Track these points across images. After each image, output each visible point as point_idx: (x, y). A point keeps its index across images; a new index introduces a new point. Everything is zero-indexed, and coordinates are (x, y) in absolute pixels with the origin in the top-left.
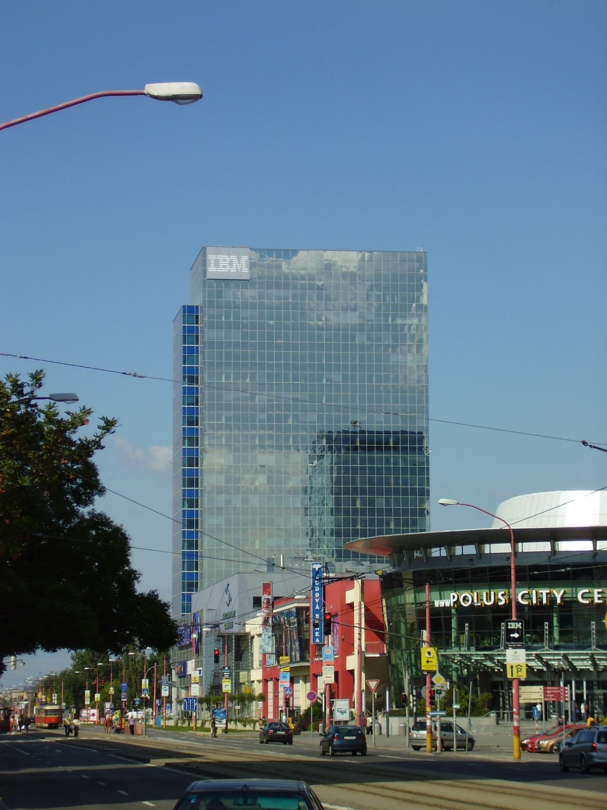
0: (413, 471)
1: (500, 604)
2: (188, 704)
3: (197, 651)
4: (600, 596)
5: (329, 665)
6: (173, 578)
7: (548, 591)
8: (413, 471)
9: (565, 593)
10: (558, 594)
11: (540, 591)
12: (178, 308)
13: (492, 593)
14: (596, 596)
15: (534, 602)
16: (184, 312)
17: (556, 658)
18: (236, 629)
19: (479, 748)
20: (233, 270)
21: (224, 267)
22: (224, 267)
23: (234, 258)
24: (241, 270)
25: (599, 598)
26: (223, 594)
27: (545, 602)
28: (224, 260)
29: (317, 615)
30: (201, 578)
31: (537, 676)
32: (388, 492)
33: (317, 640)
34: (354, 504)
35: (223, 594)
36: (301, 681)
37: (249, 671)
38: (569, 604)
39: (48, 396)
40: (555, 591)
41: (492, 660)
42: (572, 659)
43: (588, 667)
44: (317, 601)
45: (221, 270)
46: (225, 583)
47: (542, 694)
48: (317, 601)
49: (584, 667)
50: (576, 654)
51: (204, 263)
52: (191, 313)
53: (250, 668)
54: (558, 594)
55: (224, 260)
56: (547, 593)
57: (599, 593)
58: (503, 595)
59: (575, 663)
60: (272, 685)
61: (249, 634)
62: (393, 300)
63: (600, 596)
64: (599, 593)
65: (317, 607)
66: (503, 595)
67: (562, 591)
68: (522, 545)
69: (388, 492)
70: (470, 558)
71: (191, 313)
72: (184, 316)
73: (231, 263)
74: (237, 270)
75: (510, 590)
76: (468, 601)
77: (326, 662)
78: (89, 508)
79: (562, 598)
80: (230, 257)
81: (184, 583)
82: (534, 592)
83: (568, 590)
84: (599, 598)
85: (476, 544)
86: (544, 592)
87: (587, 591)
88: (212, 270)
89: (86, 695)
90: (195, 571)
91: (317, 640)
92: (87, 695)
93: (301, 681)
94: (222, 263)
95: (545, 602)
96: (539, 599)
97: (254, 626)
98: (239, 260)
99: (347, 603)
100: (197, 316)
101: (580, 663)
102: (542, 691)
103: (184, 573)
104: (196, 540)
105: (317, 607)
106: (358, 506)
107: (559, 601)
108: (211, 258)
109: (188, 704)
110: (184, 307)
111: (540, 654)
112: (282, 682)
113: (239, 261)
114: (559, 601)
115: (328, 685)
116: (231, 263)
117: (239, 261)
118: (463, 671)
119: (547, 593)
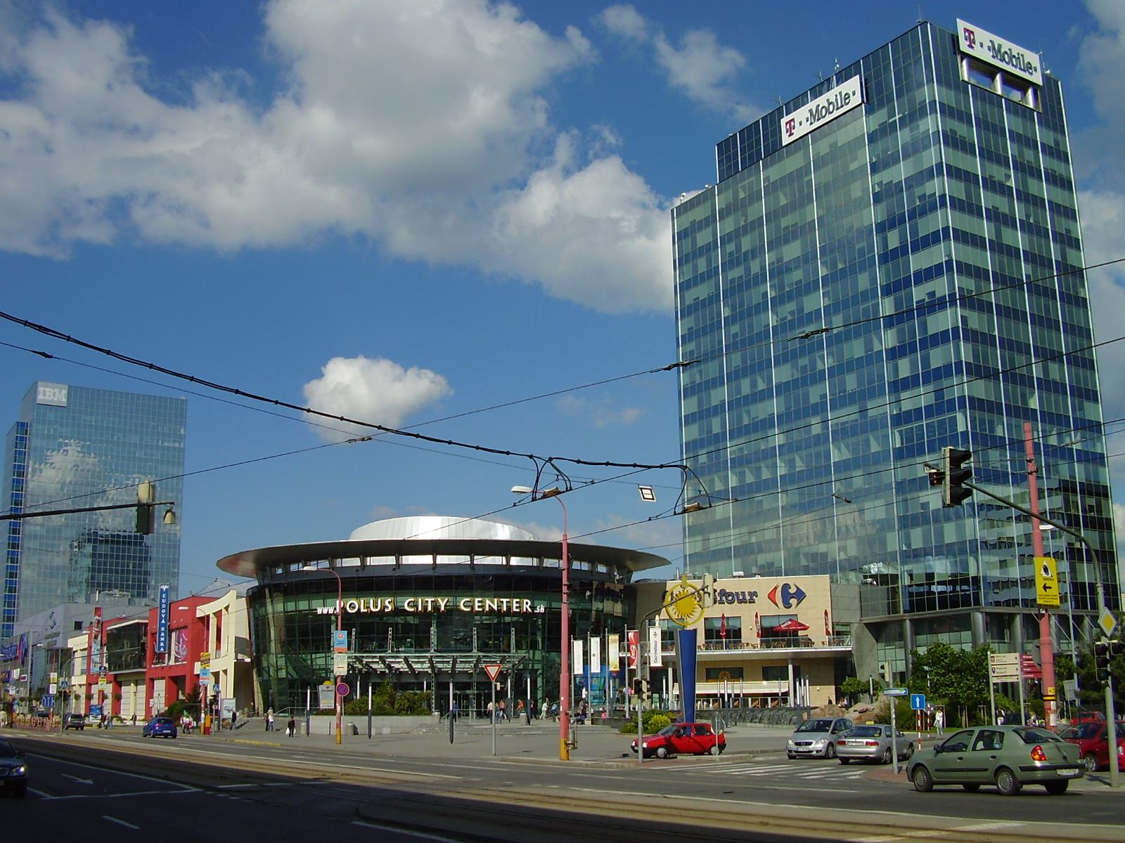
0: (169, 547)
1: (386, 610)
2: (47, 701)
3: (23, 662)
4: (480, 604)
5: (341, 653)
7: (433, 599)
8: (169, 547)
9: (448, 601)
10: (442, 603)
11: (426, 599)
12: (13, 423)
13: (379, 601)
14: (477, 604)
15: (420, 609)
16: (18, 426)
17: (397, 660)
18: (59, 645)
19: (815, 753)
20: (55, 399)
23: (56, 390)
25: (479, 607)
26: (47, 620)
27: (429, 609)
29: (163, 629)
30: (17, 613)
31: (380, 678)
32: (105, 571)
33: (162, 649)
34: (128, 566)
35: (47, 620)
36: (132, 684)
37: (268, 655)
38: (452, 611)
40: (439, 599)
41: (361, 662)
42: (412, 662)
43: (425, 670)
44: (163, 616)
45: (47, 398)
46: (50, 612)
47: (1018, 667)
48: (163, 616)
49: (422, 670)
50: (464, 657)
51: (36, 393)
52: (22, 426)
54: (442, 603)
56: (432, 601)
57: (479, 602)
58: (389, 602)
59: (415, 666)
60: (164, 684)
61: (71, 649)
62: (163, 430)
63: (480, 604)
64: (479, 602)
65: (163, 622)
66: (389, 602)
67: (446, 600)
69: (105, 571)
70: (356, 569)
71: (22, 426)
72: (18, 429)
73: (54, 394)
76: (354, 608)
77: (338, 649)
79: (445, 606)
81: (4, 616)
82: (420, 600)
83: (451, 599)
84: (479, 607)
85: (361, 556)
86: (430, 600)
87: (469, 599)
88: (41, 398)
90: (13, 608)
91: (162, 649)
93: (132, 684)
95: (429, 609)
96: (425, 608)
97: (78, 643)
98: (60, 392)
99: (198, 616)
100: (27, 430)
101: (419, 666)
102: (1018, 661)
105: (163, 622)
106: (131, 568)
107: (443, 609)
108: (41, 389)
109: (47, 701)
110: (18, 422)
111: (384, 656)
112: (202, 679)
113: (60, 394)
114: (443, 609)
115: (340, 678)
116: (54, 394)
117: (60, 394)
119: (432, 601)
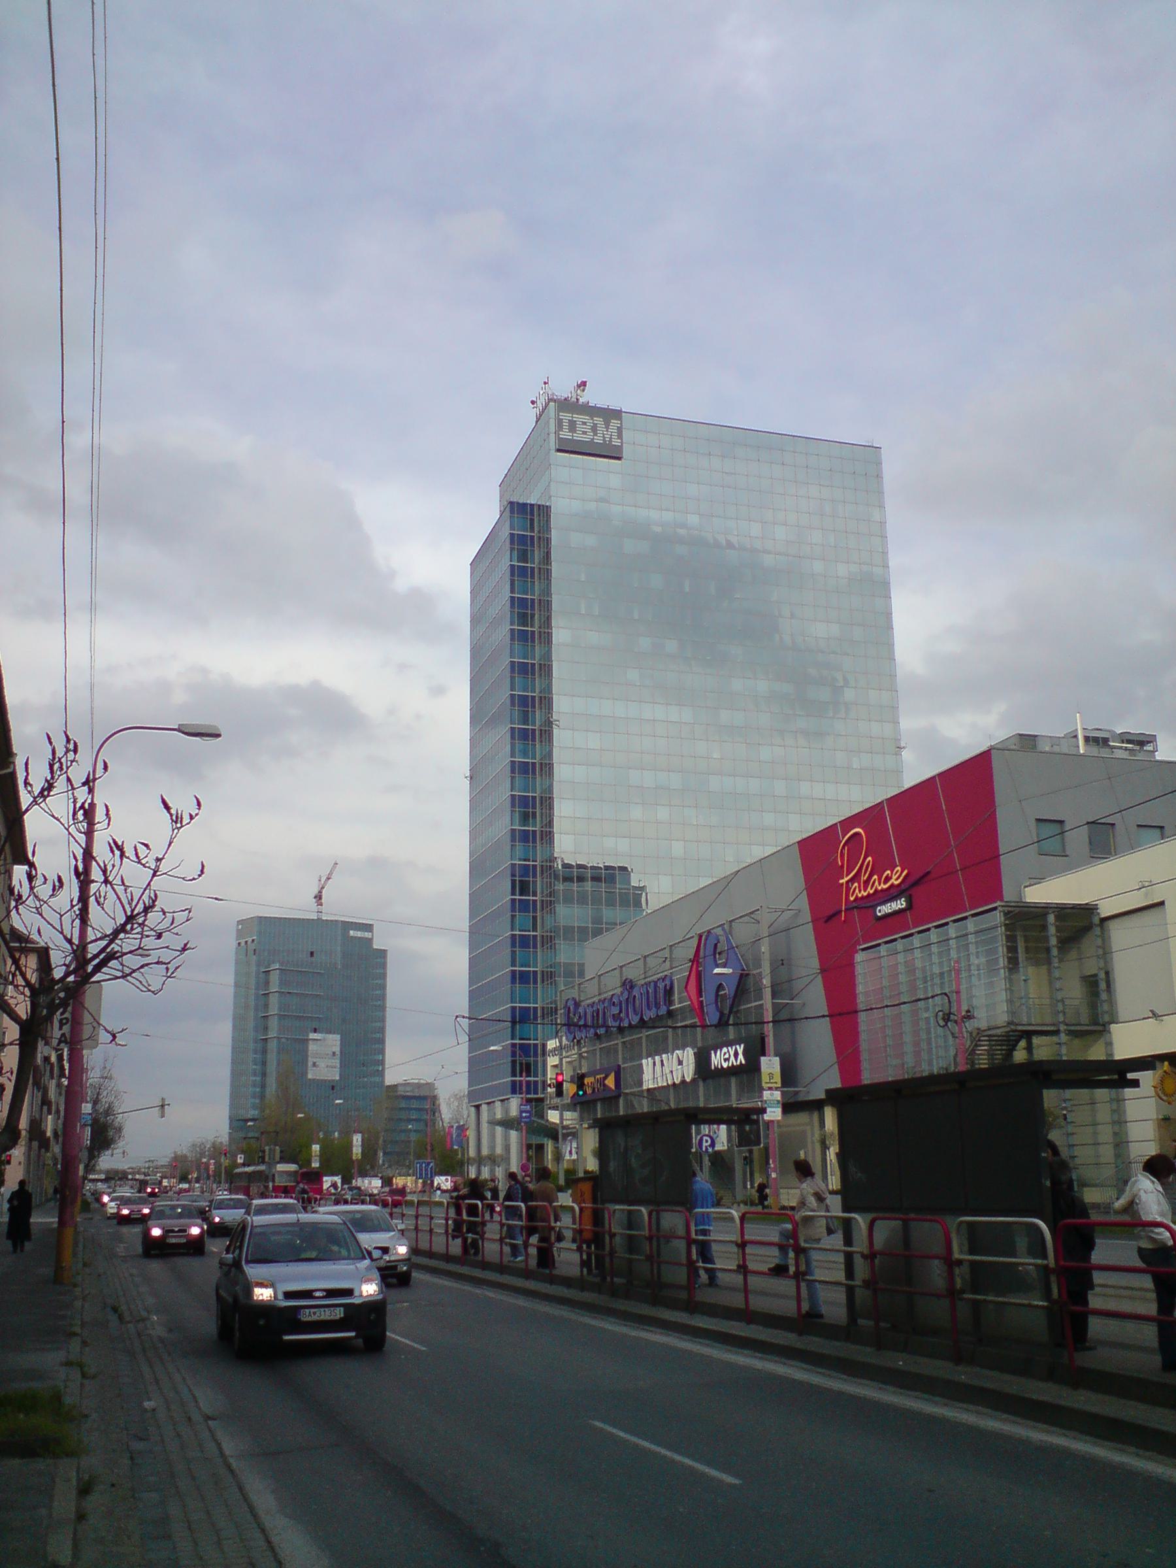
6: (470, 991)
21: (584, 433)
22: (584, 433)
24: (610, 441)
28: (584, 423)
39: (176, 727)
53: (1107, 1018)
55: (584, 423)
68: (824, 1016)
74: (604, 440)
75: (1105, 912)
78: (356, 1174)
80: (592, 419)
89: (863, 1037)
92: (771, 1075)
94: (580, 427)
103: (513, 936)
104: (516, 947)
113: (607, 428)
116: (594, 429)
117: (607, 428)
118: (488, 1258)
